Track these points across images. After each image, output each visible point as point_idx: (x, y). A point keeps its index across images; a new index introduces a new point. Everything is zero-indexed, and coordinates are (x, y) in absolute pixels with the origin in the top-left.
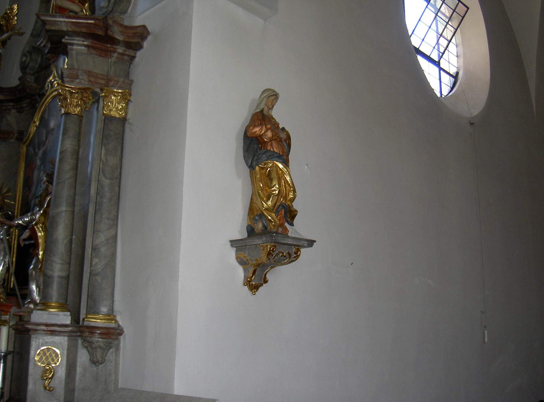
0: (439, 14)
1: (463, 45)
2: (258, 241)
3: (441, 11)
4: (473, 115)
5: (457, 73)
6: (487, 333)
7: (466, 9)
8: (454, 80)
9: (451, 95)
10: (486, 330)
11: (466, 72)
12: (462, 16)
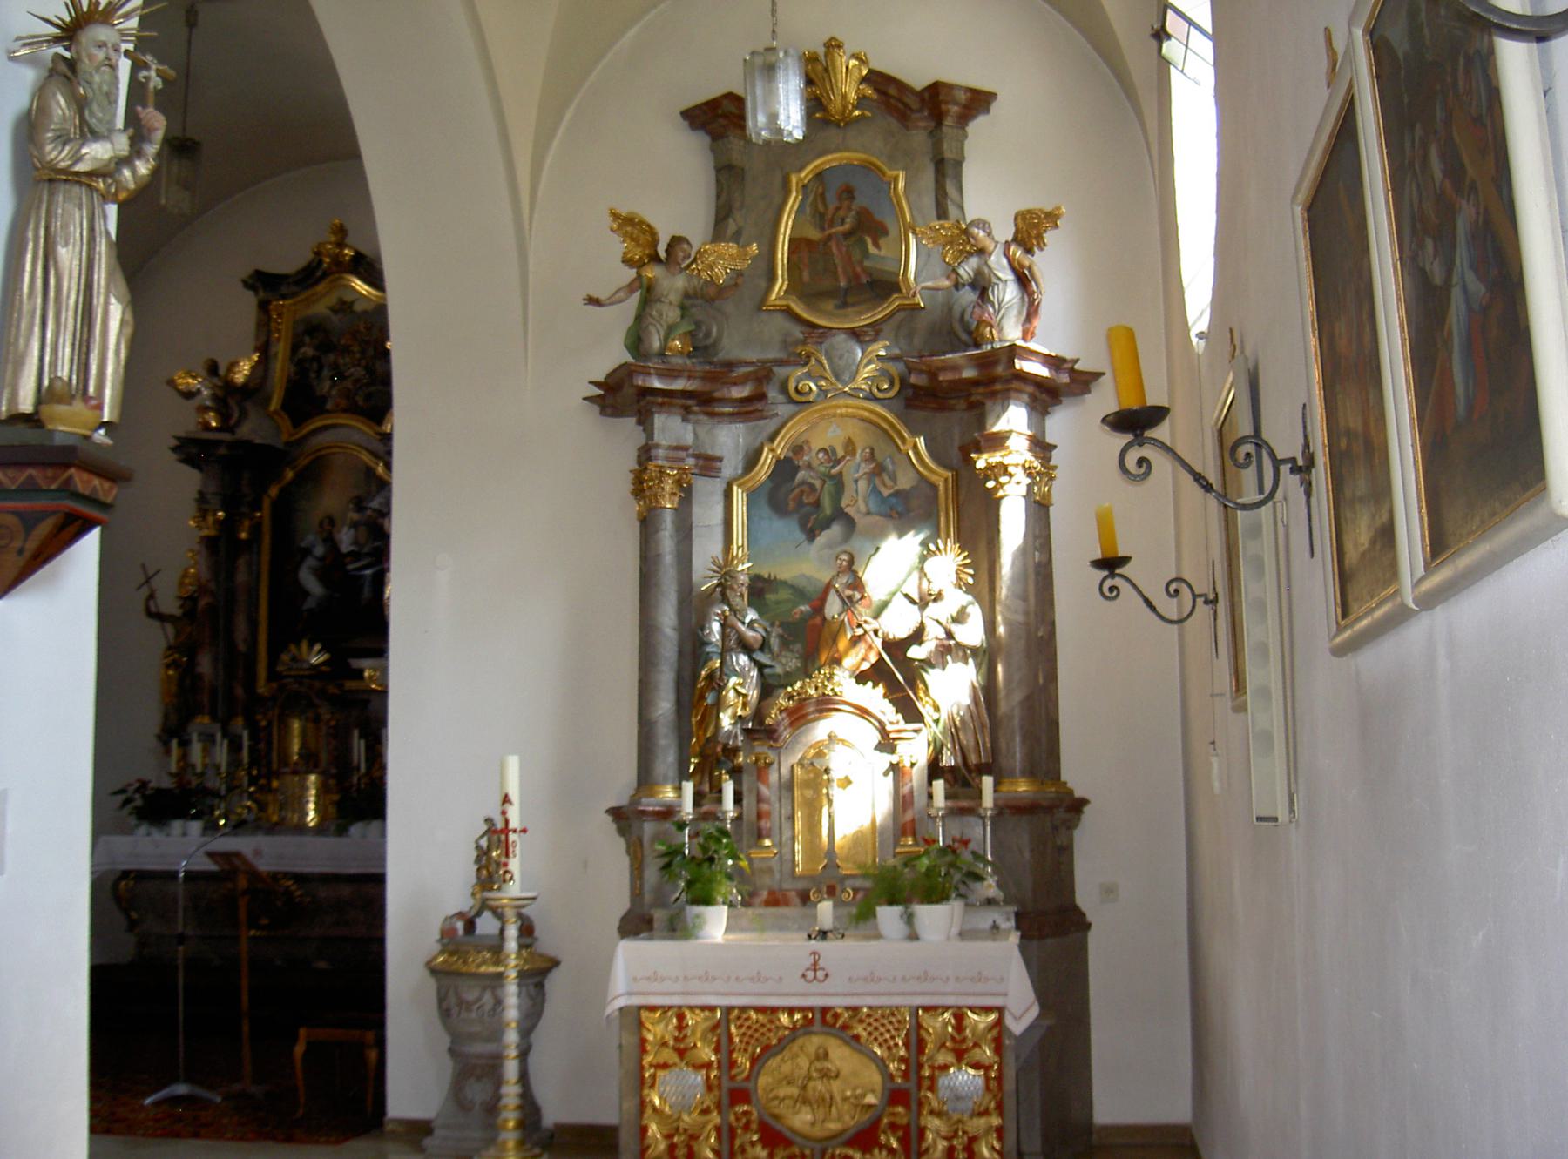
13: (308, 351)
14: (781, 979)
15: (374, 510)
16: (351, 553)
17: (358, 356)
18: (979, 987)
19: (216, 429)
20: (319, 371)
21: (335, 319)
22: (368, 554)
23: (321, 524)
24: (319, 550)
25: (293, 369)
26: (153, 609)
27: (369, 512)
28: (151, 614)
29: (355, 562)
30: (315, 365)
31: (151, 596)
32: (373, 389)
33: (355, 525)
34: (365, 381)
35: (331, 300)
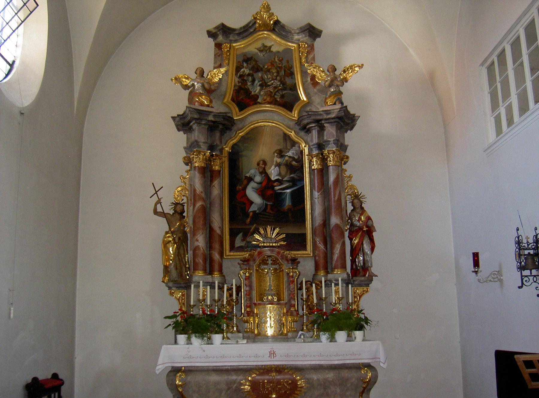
0: (10, 4)
1: (24, 37)
2: (322, 245)
3: (12, 2)
4: (24, 106)
5: (14, 62)
6: (13, 310)
7: (36, 5)
8: (10, 68)
9: (6, 82)
10: (12, 307)
11: (22, 63)
12: (31, 11)
13: (246, 71)
14: (264, 356)
15: (290, 157)
16: (277, 180)
17: (275, 74)
18: (321, 358)
19: (208, 106)
20: (253, 81)
21: (261, 55)
22: (288, 181)
23: (258, 164)
24: (258, 179)
25: (237, 80)
26: (159, 209)
27: (287, 158)
28: (156, 212)
29: (280, 185)
30: (250, 78)
31: (159, 202)
32: (284, 92)
33: (278, 165)
34: (280, 88)
35: (259, 45)
